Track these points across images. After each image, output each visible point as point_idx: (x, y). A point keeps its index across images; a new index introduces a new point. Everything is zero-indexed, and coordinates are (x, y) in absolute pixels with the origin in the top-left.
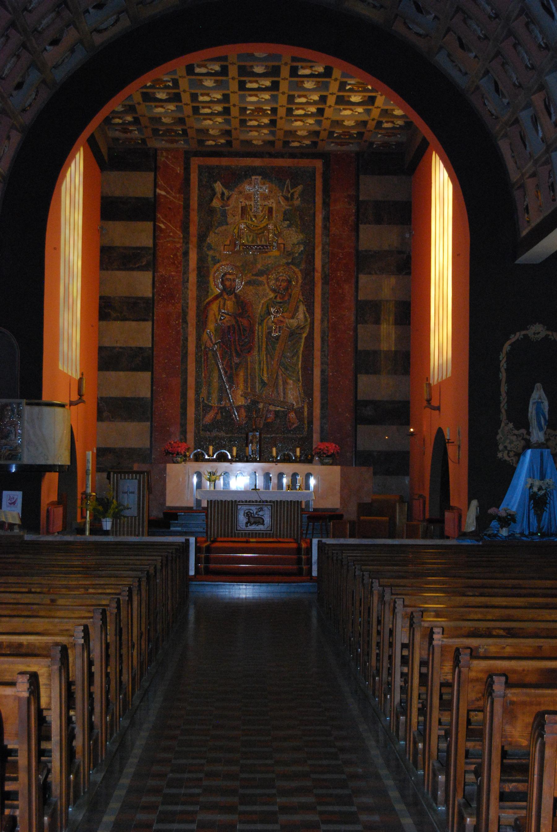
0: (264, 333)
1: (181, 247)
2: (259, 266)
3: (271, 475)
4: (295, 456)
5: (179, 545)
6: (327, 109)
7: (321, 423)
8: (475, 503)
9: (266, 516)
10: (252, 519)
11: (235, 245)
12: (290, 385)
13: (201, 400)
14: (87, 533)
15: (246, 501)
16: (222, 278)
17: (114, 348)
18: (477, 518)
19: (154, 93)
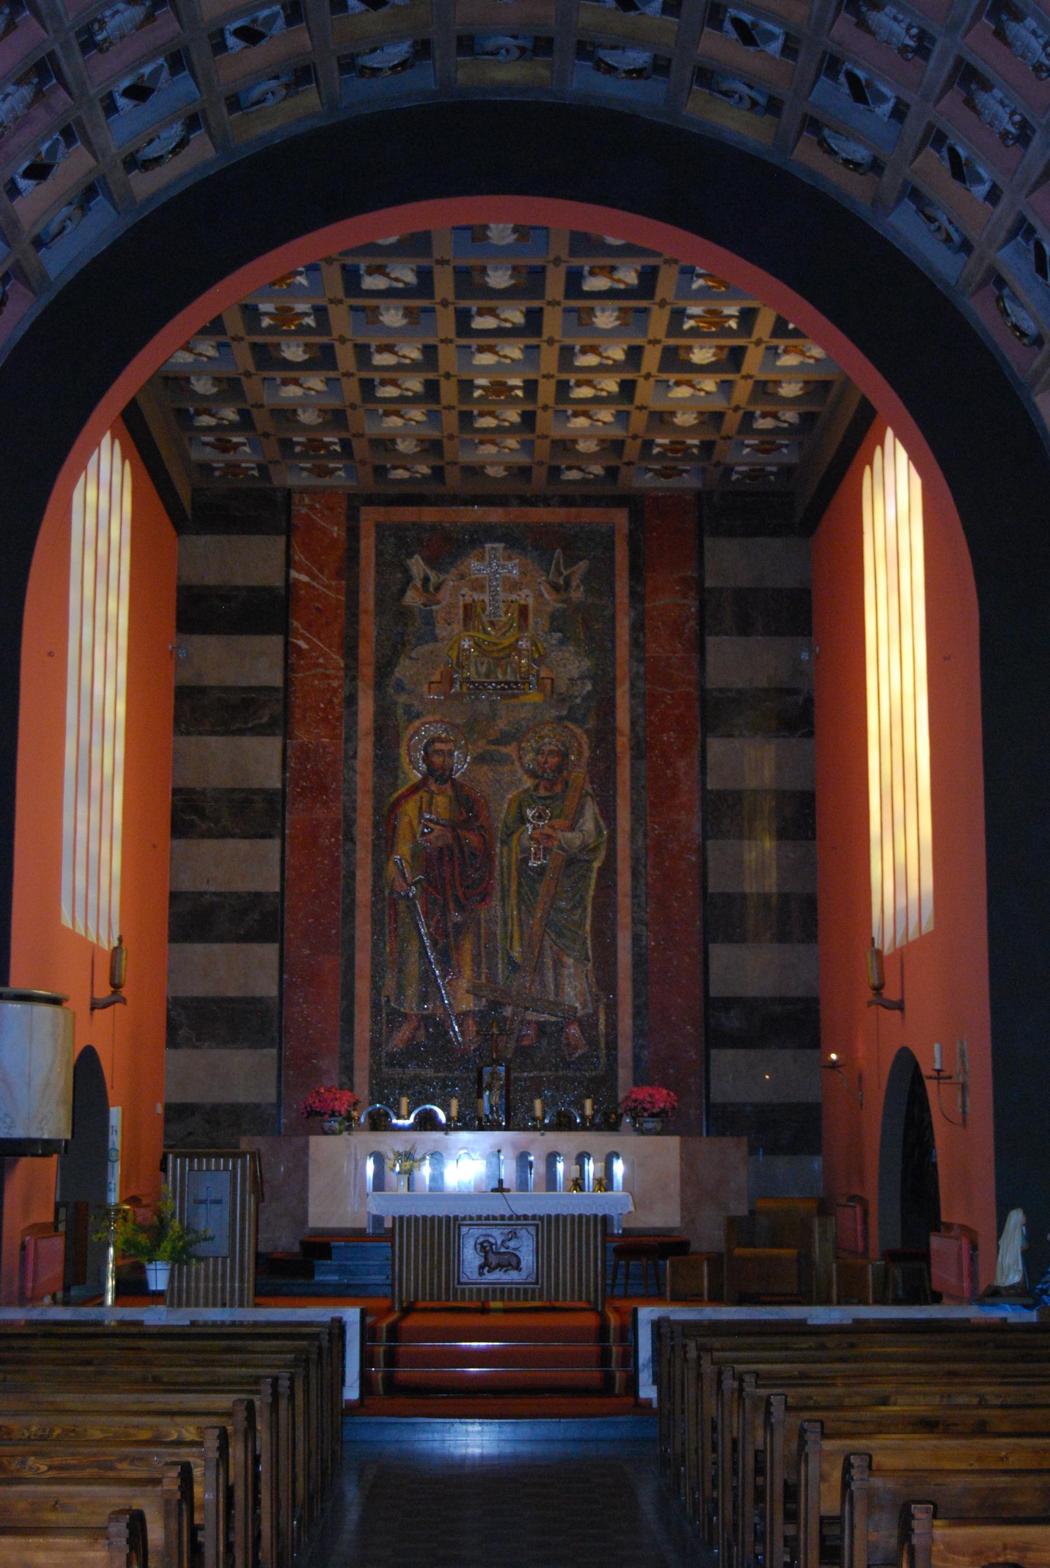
0: (514, 860)
1: (340, 686)
2: (501, 725)
3: (532, 1158)
4: (583, 1117)
5: (315, 1336)
6: (641, 381)
7: (634, 1048)
8: (1016, 1218)
9: (523, 1249)
10: (495, 1258)
11: (452, 682)
12: (569, 968)
13: (383, 1000)
14: (109, 1299)
15: (479, 1218)
16: (425, 750)
17: (201, 894)
18: (1025, 1254)
19: (278, 345)
